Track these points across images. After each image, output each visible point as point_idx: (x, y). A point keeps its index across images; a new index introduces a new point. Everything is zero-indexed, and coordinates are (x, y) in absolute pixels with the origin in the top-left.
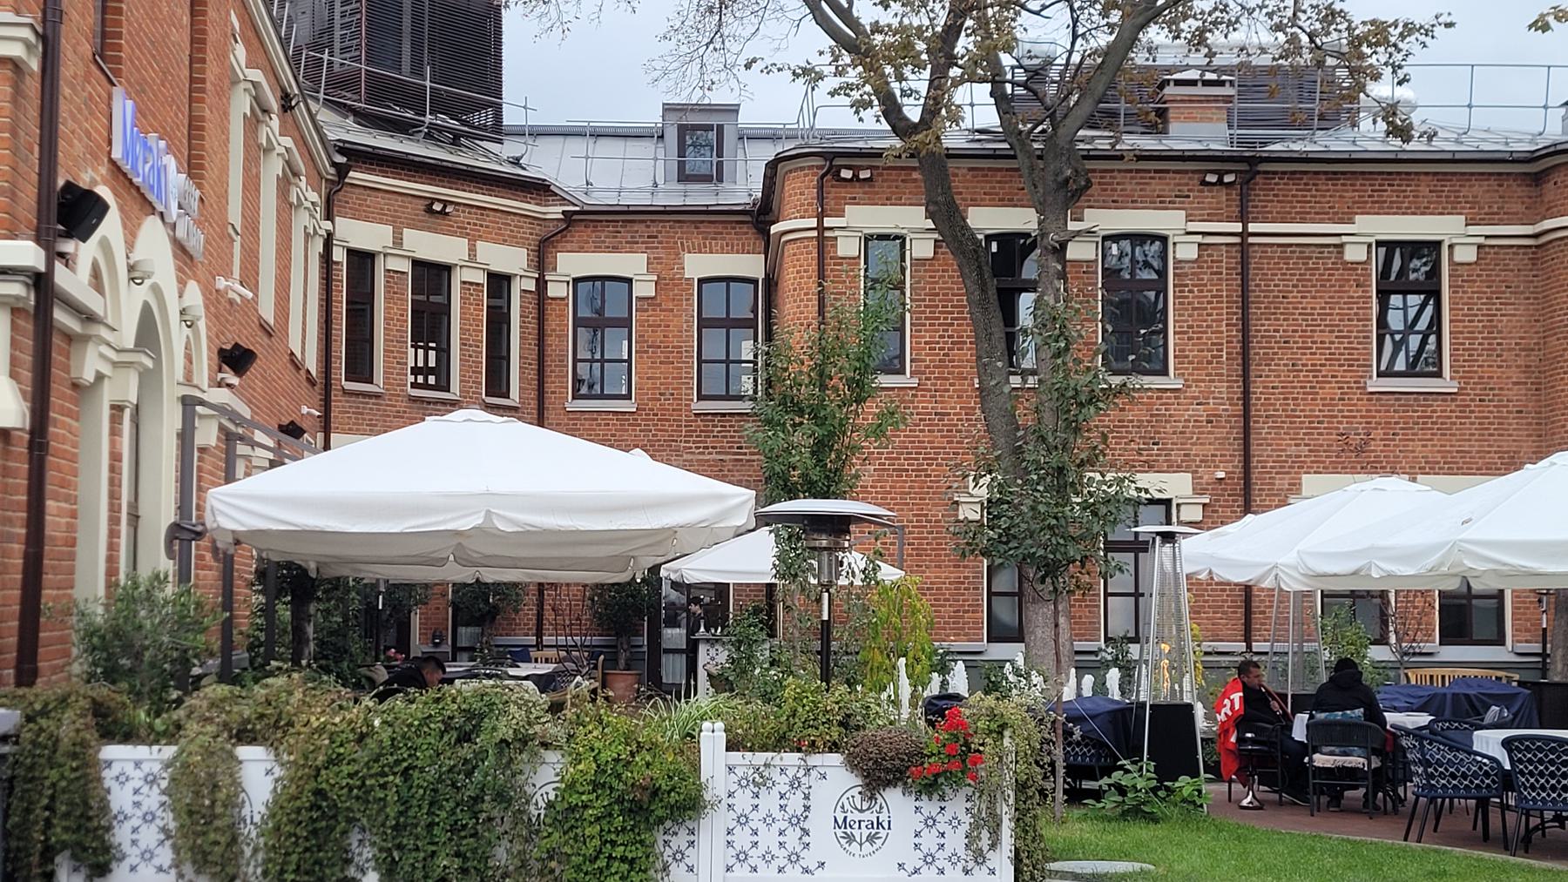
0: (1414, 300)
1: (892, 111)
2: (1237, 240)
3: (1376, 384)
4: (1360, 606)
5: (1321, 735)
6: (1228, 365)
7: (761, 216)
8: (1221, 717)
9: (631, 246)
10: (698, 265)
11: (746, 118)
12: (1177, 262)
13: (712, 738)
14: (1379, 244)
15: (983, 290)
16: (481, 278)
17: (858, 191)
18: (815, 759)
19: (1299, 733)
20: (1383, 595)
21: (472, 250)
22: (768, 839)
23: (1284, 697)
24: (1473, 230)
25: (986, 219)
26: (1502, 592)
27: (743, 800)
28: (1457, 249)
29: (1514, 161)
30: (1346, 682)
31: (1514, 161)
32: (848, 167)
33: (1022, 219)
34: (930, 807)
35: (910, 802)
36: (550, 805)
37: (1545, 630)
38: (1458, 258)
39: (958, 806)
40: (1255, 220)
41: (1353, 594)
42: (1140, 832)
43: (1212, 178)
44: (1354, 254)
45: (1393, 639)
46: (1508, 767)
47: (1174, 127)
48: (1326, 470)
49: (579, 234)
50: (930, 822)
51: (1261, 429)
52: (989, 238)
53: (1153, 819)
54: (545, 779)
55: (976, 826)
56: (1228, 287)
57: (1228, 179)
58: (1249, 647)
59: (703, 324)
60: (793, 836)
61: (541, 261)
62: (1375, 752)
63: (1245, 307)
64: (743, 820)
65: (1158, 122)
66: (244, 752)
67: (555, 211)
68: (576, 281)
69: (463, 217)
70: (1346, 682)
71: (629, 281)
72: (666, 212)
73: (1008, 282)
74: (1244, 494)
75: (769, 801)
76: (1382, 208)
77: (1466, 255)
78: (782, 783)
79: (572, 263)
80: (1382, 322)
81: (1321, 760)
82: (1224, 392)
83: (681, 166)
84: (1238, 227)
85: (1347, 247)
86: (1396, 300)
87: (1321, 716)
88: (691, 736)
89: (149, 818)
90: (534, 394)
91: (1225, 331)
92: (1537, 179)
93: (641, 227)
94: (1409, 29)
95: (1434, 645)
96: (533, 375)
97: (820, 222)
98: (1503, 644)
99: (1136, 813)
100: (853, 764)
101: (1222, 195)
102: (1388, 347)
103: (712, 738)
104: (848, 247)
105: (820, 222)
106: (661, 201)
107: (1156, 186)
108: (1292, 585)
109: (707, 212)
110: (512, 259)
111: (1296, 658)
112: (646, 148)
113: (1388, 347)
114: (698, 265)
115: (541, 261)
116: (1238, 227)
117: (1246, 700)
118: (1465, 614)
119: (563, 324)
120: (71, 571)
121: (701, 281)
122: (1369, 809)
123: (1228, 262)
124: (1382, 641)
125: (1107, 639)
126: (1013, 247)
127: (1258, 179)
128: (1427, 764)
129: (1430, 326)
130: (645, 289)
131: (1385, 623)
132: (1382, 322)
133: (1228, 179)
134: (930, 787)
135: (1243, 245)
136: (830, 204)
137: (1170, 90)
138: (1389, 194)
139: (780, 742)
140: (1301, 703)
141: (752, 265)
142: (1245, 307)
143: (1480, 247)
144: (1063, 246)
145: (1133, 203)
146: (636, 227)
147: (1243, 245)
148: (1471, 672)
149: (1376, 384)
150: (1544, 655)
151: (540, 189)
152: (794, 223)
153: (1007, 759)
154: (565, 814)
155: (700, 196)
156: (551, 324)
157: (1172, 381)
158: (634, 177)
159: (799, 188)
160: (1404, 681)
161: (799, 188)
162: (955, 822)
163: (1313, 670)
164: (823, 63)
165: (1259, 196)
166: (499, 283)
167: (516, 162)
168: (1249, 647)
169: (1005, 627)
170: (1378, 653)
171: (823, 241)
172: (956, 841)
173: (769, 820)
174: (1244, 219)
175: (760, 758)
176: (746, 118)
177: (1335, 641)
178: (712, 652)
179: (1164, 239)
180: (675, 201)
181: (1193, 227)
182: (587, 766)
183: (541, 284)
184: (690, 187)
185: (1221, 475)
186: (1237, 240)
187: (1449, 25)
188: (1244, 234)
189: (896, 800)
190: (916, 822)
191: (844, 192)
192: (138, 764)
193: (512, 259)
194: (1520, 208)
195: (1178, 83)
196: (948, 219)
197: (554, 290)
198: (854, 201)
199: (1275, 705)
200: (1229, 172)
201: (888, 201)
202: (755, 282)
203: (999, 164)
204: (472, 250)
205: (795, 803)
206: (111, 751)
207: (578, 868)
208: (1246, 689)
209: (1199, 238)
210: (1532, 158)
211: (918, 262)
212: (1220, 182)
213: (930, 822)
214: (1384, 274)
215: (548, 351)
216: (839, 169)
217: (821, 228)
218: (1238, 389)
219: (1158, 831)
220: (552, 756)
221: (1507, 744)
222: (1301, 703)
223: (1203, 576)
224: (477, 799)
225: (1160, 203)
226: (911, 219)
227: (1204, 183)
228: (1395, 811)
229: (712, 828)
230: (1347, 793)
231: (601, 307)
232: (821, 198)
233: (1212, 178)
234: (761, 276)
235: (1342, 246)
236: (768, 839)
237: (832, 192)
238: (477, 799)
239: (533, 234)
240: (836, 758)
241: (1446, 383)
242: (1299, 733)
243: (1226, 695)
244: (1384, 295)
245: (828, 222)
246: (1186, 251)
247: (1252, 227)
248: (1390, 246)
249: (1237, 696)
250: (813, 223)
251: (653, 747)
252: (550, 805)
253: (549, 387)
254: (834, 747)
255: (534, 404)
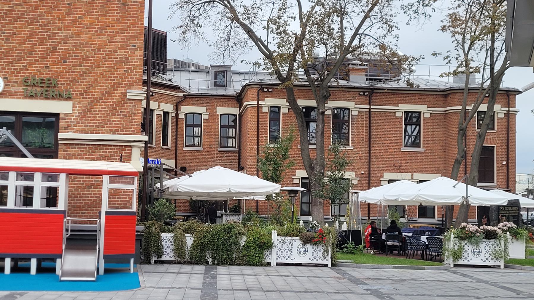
0: (414, 127)
1: (280, 76)
2: (368, 110)
3: (404, 149)
4: (399, 209)
5: (388, 238)
6: (365, 144)
7: (238, 99)
8: (366, 234)
9: (202, 105)
10: (220, 110)
11: (233, 69)
12: (352, 115)
13: (274, 234)
14: (405, 112)
15: (303, 123)
16: (161, 113)
17: (268, 94)
18: (294, 238)
19: (384, 237)
20: (404, 206)
21: (159, 105)
22: (284, 253)
23: (380, 229)
24: (429, 109)
25: (302, 103)
26: (434, 206)
27: (280, 246)
28: (425, 114)
29: (440, 91)
30: (394, 226)
31: (440, 91)
32: (266, 88)
33: (312, 103)
34: (315, 247)
35: (312, 247)
36: (243, 246)
37: (293, 212)
38: (425, 116)
39: (321, 247)
40: (373, 105)
41: (396, 206)
42: (351, 256)
43: (362, 93)
44: (399, 114)
45: (406, 216)
46: (427, 243)
47: (351, 77)
48: (390, 172)
49: (188, 101)
50: (315, 250)
51: (373, 160)
52: (303, 108)
53: (354, 254)
54: (243, 241)
55: (324, 251)
56: (366, 122)
57: (366, 94)
58: (369, 218)
59: (222, 126)
60: (289, 253)
61: (177, 108)
62: (401, 242)
63: (370, 128)
64: (280, 249)
65: (346, 77)
66: (186, 235)
67: (181, 94)
68: (186, 114)
69: (157, 96)
70: (394, 226)
71: (201, 114)
72: (212, 95)
73: (308, 119)
74: (370, 181)
75: (285, 246)
76: (406, 103)
77: (427, 115)
78: (287, 242)
79: (185, 109)
80: (406, 130)
81: (388, 243)
82: (364, 151)
83: (215, 82)
84: (368, 107)
85: (397, 113)
86: (409, 127)
87: (388, 233)
88: (270, 233)
89: (168, 247)
90: (174, 145)
91: (364, 134)
92: (446, 96)
93: (205, 99)
94: (414, 59)
95: (417, 218)
96: (174, 140)
97: (258, 102)
98: (434, 218)
99: (351, 252)
100: (301, 239)
101: (365, 98)
102: (407, 137)
103: (274, 234)
104: (266, 109)
105: (258, 102)
106: (210, 92)
107: (347, 95)
108: (384, 204)
109: (223, 96)
110: (169, 108)
111: (383, 220)
112: (203, 76)
113: (407, 137)
114: (220, 110)
115: (177, 108)
116: (368, 107)
117: (372, 230)
118: (425, 211)
119: (182, 126)
120: (109, 198)
121: (221, 115)
122: (399, 255)
123: (366, 116)
124: (404, 217)
125: (332, 216)
126: (309, 109)
127: (374, 94)
128: (411, 243)
129: (417, 134)
130: (205, 117)
131: (404, 212)
132: (406, 130)
133: (366, 94)
134: (316, 244)
135: (370, 111)
136: (261, 97)
137: (350, 66)
138: (408, 99)
139: (287, 235)
140: (384, 231)
141: (235, 111)
142: (370, 128)
143: (431, 113)
144: (324, 112)
145: (341, 100)
146: (203, 99)
147: (370, 111)
148: (423, 225)
149: (404, 149)
150: (443, 221)
151: (177, 88)
152: (250, 102)
153: (331, 239)
154: (247, 247)
155: (221, 91)
156: (179, 126)
157: (350, 147)
158: (198, 84)
159: (252, 93)
160: (408, 227)
161: (252, 93)
162: (320, 251)
163: (386, 224)
164: (261, 62)
165: (374, 98)
166: (166, 114)
167: (170, 80)
168: (369, 218)
169: (305, 212)
170: (402, 220)
171: (259, 107)
172: (320, 254)
173: (285, 250)
174: (370, 104)
175: (283, 238)
176: (233, 69)
177: (392, 217)
178: (226, 217)
179: (349, 109)
180: (214, 93)
181: (357, 106)
182: (251, 238)
183: (177, 114)
184: (218, 88)
185: (363, 172)
186: (368, 110)
187: (423, 58)
188: (370, 109)
189: (308, 245)
190: (313, 250)
191: (265, 95)
192: (166, 237)
193: (169, 108)
194: (441, 103)
195: (353, 64)
196: (292, 103)
197: (180, 116)
198: (267, 97)
199: (378, 231)
200: (366, 92)
201: (276, 97)
202: (235, 115)
203: (308, 89)
204: (159, 105)
205: (290, 247)
206: (163, 234)
207: (250, 258)
208: (372, 227)
209: (358, 109)
210: (444, 90)
211: (284, 114)
212: (364, 94)
213: (315, 250)
214: (405, 120)
215: (179, 133)
216: (263, 89)
217: (258, 104)
218: (367, 150)
219: (356, 256)
220: (244, 237)
221: (427, 238)
222: (384, 231)
223: (363, 202)
224: (231, 245)
225: (348, 100)
226: (282, 102)
227: (360, 95)
228: (405, 255)
229: (274, 251)
230: (394, 252)
231: (194, 121)
232: (258, 96)
233: (362, 93)
234: (238, 114)
235: (395, 112)
236: (284, 253)
237: (261, 94)
238: (231, 245)
239: (175, 101)
240: (298, 238)
241: (421, 149)
242: (384, 237)
243: (367, 229)
244: (406, 125)
245: (260, 103)
246: (355, 113)
247: (372, 107)
248: (407, 113)
249: (370, 229)
250: (256, 102)
251: (264, 235)
252: (243, 246)
253: (179, 143)
254: (297, 236)
255: (174, 148)
